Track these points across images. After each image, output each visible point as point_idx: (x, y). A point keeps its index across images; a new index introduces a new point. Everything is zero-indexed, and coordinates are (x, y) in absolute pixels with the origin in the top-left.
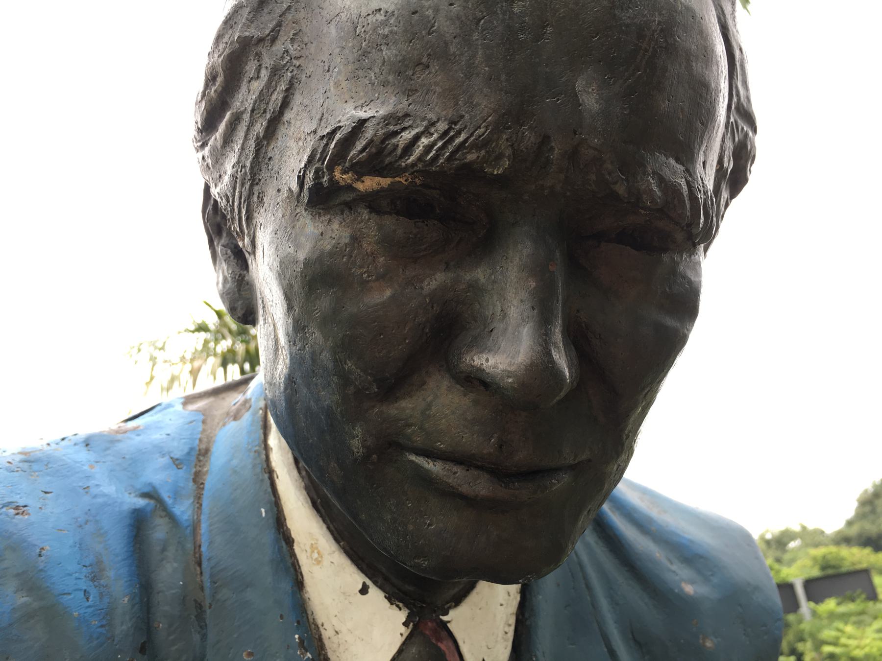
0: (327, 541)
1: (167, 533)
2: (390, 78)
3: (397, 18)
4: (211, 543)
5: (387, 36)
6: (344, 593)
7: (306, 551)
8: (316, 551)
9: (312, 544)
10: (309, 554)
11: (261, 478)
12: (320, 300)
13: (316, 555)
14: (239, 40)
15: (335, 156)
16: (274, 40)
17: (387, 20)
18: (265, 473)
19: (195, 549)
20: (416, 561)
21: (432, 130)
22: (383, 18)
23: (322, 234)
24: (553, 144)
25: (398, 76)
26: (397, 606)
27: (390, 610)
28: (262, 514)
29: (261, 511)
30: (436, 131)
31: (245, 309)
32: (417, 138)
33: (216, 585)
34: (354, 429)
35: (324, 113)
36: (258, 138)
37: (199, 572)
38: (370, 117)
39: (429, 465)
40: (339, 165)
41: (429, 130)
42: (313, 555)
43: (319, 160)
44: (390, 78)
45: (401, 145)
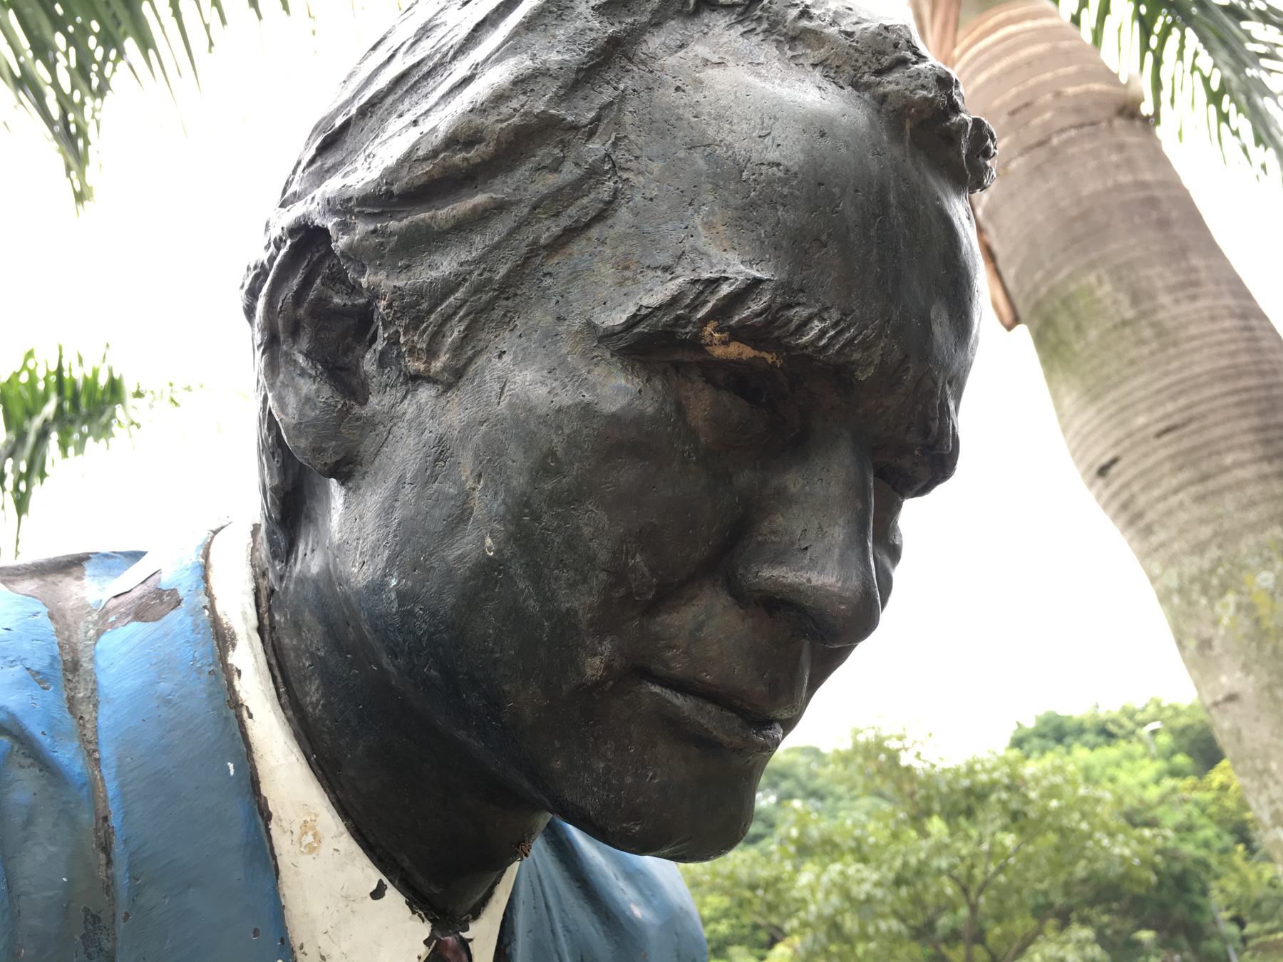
0: (333, 817)
1: (35, 794)
2: (785, 243)
3: (801, 182)
4: (126, 814)
5: (786, 196)
6: (346, 897)
7: (292, 832)
8: (310, 833)
9: (305, 822)
10: (295, 837)
11: (225, 715)
12: (619, 471)
13: (309, 839)
14: (541, 116)
15: (717, 310)
16: (591, 135)
17: (788, 179)
18: (231, 708)
19: (97, 822)
20: (624, 825)
21: (826, 316)
22: (780, 174)
23: (640, 391)
24: (910, 365)
25: (793, 244)
26: (420, 916)
27: (411, 922)
28: (229, 771)
29: (228, 767)
30: (830, 317)
31: (342, 455)
32: (810, 319)
33: (138, 882)
34: (600, 644)
35: (1109, 325)
36: (535, 242)
37: (103, 862)
38: (767, 280)
39: (678, 700)
40: (717, 320)
41: (822, 314)
42: (303, 838)
43: (686, 307)
44: (785, 243)
45: (796, 322)
